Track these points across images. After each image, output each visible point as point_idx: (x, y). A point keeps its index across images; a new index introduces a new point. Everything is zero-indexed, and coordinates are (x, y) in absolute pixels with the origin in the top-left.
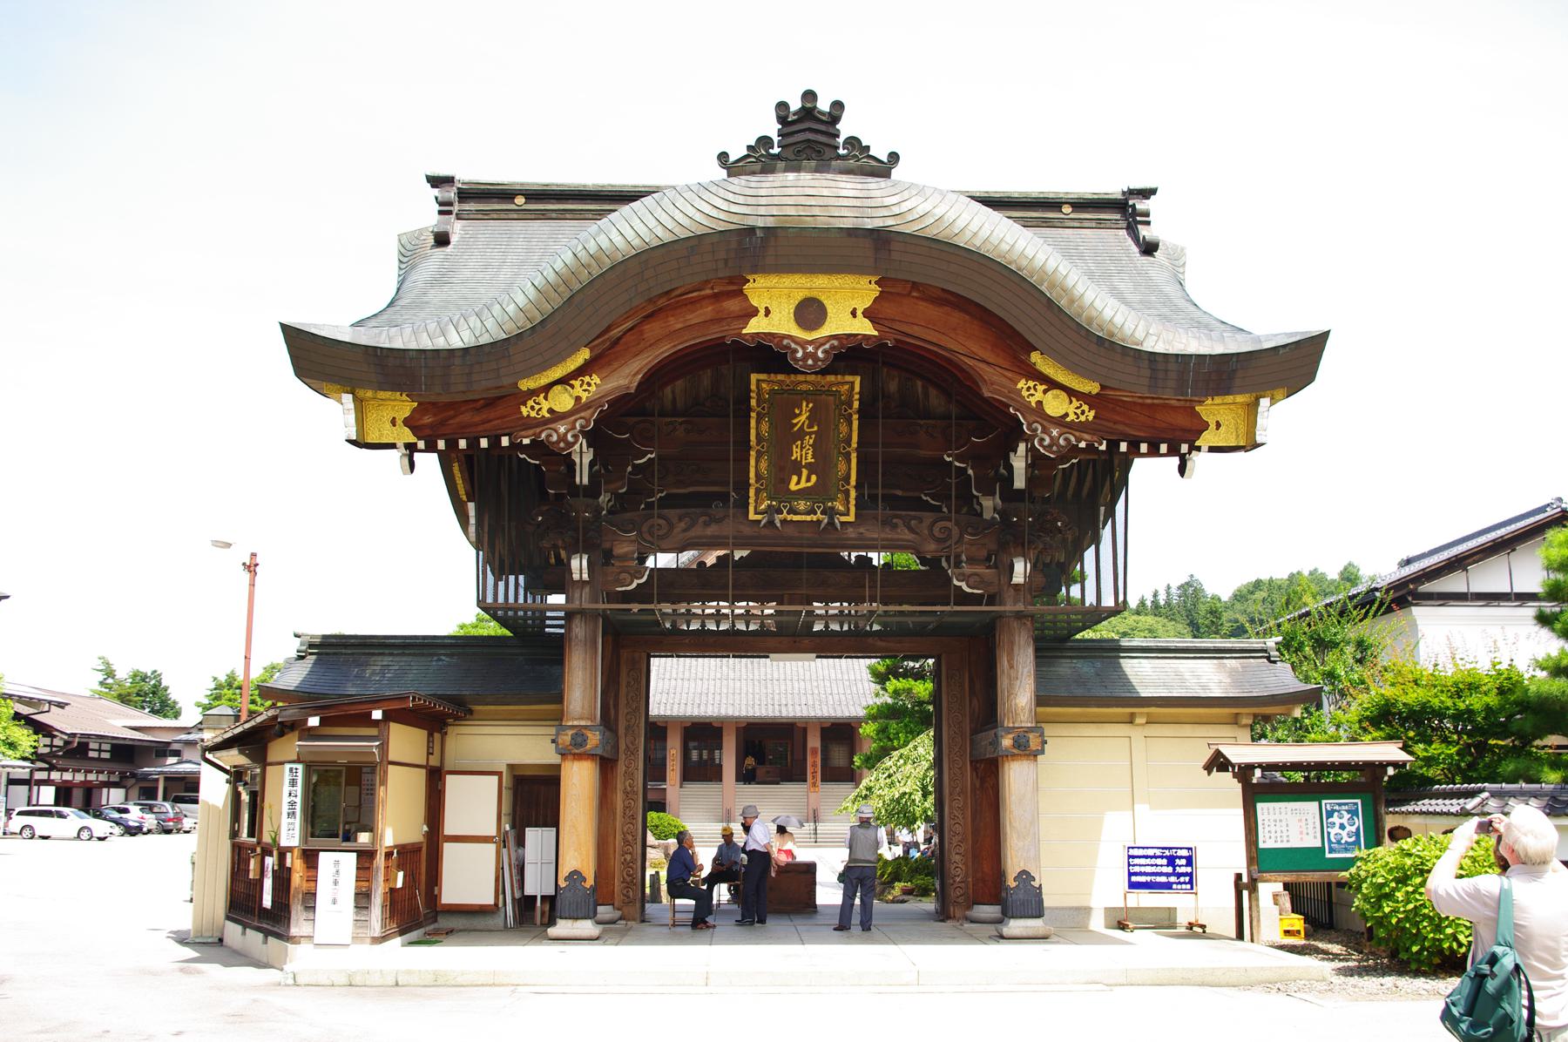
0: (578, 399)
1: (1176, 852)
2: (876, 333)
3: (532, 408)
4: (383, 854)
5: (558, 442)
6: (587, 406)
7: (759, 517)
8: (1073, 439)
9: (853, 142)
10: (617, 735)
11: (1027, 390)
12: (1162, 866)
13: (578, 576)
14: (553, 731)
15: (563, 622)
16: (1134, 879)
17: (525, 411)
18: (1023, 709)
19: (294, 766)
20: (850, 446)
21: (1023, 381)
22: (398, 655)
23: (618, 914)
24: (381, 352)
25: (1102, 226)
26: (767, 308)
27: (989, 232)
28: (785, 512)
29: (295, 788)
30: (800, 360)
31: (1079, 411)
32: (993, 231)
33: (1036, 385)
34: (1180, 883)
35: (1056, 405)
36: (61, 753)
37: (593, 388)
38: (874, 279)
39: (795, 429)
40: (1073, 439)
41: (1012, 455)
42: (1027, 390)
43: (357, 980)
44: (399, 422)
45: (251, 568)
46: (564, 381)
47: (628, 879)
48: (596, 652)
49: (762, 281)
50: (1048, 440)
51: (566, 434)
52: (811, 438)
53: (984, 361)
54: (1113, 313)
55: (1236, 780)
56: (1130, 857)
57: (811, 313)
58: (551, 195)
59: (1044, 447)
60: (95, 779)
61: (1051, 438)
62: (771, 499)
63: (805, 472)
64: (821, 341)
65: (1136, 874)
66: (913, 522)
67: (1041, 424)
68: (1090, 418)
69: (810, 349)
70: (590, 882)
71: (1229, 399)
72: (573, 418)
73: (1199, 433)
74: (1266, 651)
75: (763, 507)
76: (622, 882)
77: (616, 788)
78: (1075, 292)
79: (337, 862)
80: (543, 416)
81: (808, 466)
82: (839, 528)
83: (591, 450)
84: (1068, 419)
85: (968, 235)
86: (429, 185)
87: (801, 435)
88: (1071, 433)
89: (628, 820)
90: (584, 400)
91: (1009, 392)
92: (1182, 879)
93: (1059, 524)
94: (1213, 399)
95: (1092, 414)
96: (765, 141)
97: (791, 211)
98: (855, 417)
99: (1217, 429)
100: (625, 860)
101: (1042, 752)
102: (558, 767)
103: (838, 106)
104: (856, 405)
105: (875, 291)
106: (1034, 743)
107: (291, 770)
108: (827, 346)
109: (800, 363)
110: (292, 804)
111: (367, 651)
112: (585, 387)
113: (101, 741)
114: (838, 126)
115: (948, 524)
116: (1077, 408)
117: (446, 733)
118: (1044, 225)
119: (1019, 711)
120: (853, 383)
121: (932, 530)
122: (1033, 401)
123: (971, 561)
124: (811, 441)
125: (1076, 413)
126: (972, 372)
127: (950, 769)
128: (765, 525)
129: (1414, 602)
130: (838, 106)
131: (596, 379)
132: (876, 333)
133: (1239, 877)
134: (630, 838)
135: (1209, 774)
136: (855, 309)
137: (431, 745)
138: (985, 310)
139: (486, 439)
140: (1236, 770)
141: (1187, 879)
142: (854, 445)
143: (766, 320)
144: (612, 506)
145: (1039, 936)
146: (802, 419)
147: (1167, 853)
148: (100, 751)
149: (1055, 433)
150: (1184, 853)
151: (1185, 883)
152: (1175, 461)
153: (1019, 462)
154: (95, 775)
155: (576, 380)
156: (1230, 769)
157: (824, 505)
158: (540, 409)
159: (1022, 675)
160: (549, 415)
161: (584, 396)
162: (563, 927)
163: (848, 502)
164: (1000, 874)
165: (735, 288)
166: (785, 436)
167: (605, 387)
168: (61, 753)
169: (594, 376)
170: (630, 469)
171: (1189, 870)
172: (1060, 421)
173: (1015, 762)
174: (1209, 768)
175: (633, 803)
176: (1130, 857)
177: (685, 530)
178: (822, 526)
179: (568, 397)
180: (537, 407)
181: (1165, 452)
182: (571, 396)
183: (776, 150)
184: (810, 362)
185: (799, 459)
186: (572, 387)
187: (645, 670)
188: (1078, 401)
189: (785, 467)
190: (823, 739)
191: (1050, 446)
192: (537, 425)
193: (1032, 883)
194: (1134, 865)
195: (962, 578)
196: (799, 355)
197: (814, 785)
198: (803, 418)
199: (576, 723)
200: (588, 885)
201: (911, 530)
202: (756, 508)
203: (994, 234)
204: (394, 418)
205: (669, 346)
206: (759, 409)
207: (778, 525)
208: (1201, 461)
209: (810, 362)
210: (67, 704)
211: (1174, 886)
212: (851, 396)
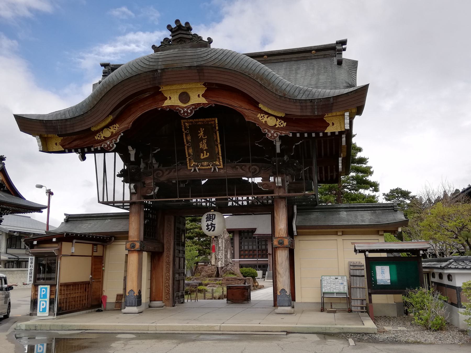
0: (112, 132)
3: (98, 137)
5: (107, 147)
7: (191, 168)
8: (279, 134)
15: (129, 207)
17: (96, 138)
19: (32, 257)
21: (259, 114)
23: (164, 304)
24: (45, 122)
25: (325, 57)
26: (170, 97)
29: (32, 265)
30: (183, 114)
31: (280, 123)
35: (271, 122)
37: (117, 129)
38: (202, 84)
39: (200, 138)
40: (279, 134)
42: (264, 119)
46: (108, 126)
47: (167, 292)
49: (165, 88)
52: (205, 140)
57: (184, 97)
61: (271, 134)
63: (205, 152)
64: (189, 106)
67: (267, 129)
68: (285, 126)
69: (185, 110)
71: (334, 114)
73: (326, 128)
74: (393, 207)
75: (218, 163)
77: (163, 261)
81: (205, 150)
84: (277, 127)
87: (202, 139)
90: (114, 133)
91: (255, 119)
93: (295, 164)
94: (328, 114)
95: (285, 123)
97: (170, 62)
98: (218, 132)
99: (333, 125)
104: (217, 128)
107: (31, 259)
112: (114, 128)
118: (305, 59)
121: (249, 170)
122: (263, 121)
124: (205, 141)
125: (279, 124)
126: (241, 113)
131: (117, 125)
132: (207, 102)
134: (168, 278)
136: (199, 94)
142: (219, 142)
143: (170, 101)
149: (272, 132)
155: (111, 126)
158: (101, 137)
160: (104, 139)
161: (114, 131)
166: (196, 141)
169: (285, 123)
170: (294, 147)
172: (274, 127)
177: (168, 174)
179: (109, 132)
180: (100, 136)
182: (110, 131)
184: (186, 114)
185: (202, 148)
186: (110, 128)
189: (198, 151)
191: (271, 137)
195: (261, 185)
196: (182, 112)
201: (243, 170)
202: (190, 165)
203: (240, 63)
204: (56, 143)
205: (140, 113)
209: (186, 114)
212: (215, 125)
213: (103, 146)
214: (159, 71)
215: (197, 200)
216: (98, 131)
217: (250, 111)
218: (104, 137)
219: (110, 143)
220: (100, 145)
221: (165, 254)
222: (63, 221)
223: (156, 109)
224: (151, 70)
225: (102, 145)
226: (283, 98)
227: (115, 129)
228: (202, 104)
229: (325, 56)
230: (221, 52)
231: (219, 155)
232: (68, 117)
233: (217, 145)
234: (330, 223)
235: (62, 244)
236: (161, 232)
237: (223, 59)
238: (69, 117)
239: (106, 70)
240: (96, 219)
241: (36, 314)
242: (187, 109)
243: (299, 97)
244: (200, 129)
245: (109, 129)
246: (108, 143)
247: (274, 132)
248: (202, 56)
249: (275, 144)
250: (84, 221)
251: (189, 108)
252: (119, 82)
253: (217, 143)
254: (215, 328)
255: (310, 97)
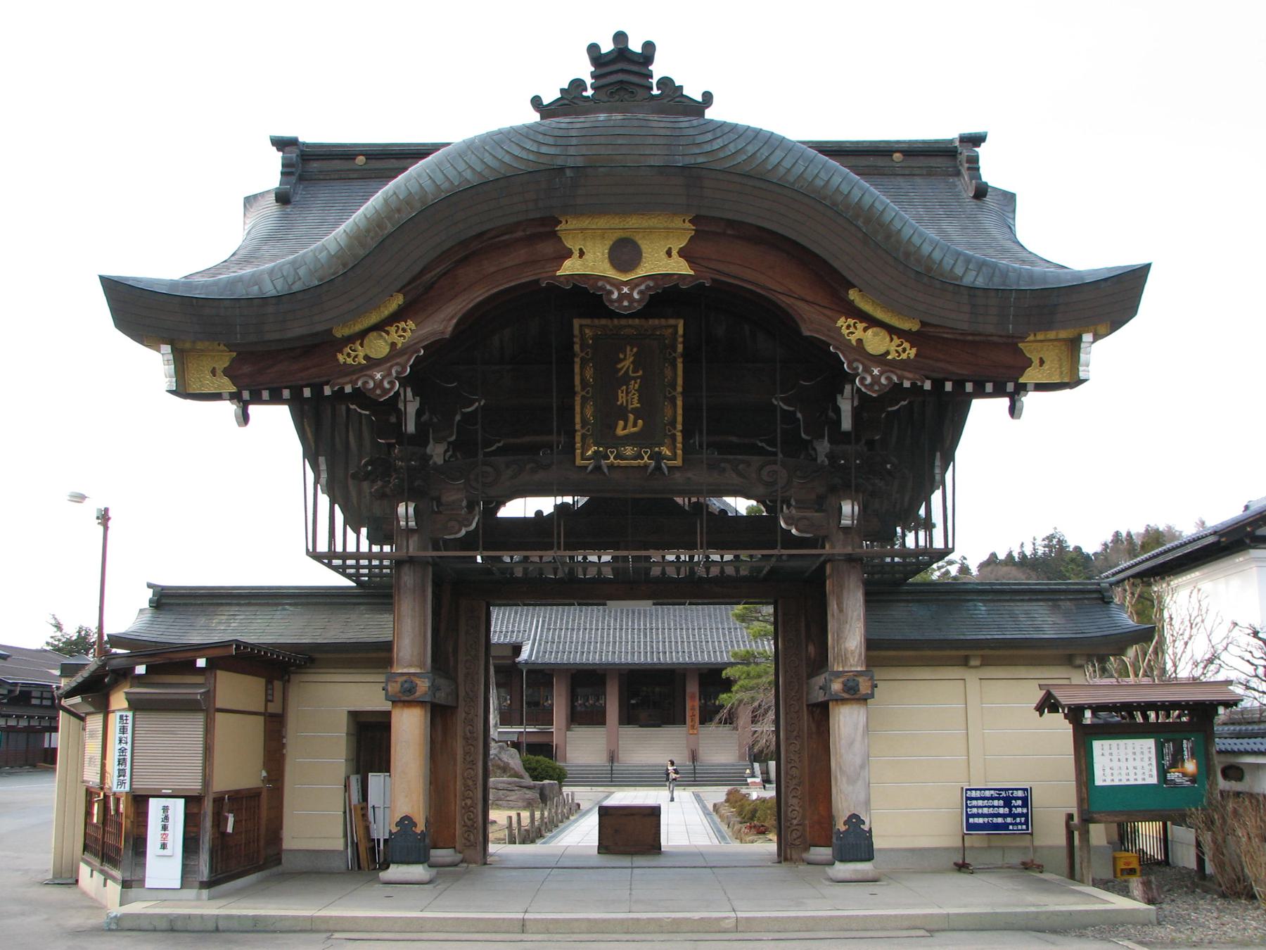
0: (393, 345)
1: (1012, 794)
2: (692, 273)
3: (349, 355)
4: (211, 800)
6: (403, 352)
8: (895, 378)
9: (666, 82)
10: (456, 683)
11: (846, 327)
12: (998, 807)
13: (404, 523)
14: (382, 678)
16: (971, 820)
18: (852, 652)
20: (675, 389)
22: (243, 605)
23: (459, 857)
27: (803, 168)
28: (612, 457)
29: (125, 735)
31: (900, 349)
32: (807, 167)
33: (856, 323)
34: (1016, 824)
35: (876, 342)
36: (5, 701)
40: (895, 378)
41: (839, 397)
43: (179, 925)
44: (219, 372)
45: (104, 518)
46: (380, 327)
47: (469, 823)
48: (425, 601)
50: (871, 379)
51: (382, 381)
52: (636, 383)
53: (802, 300)
54: (921, 241)
55: (1067, 721)
56: (968, 799)
57: (625, 253)
58: (392, 154)
59: (866, 386)
60: (37, 724)
61: (873, 376)
62: (598, 445)
63: (631, 417)
64: (636, 281)
65: (974, 816)
66: (741, 467)
67: (863, 364)
68: (912, 356)
69: (626, 290)
70: (421, 827)
71: (1052, 335)
72: (389, 364)
73: (1022, 370)
75: (590, 453)
76: (464, 826)
78: (893, 228)
79: (165, 809)
80: (359, 363)
81: (634, 411)
82: (666, 473)
83: (418, 398)
84: (889, 357)
85: (781, 171)
86: (275, 148)
87: (626, 380)
88: (892, 372)
89: (468, 766)
90: (399, 345)
92: (1018, 820)
93: (889, 466)
94: (1035, 335)
95: (914, 351)
96: (577, 84)
97: (603, 151)
98: (680, 360)
99: (1041, 365)
100: (466, 804)
101: (872, 696)
102: (388, 714)
103: (649, 47)
104: (680, 348)
105: (688, 230)
106: (864, 688)
107: (121, 717)
108: (643, 287)
109: (616, 304)
110: (123, 751)
111: (215, 601)
112: (401, 333)
113: (41, 689)
114: (650, 68)
115: (775, 467)
116: (898, 346)
117: (289, 681)
119: (849, 655)
120: (676, 327)
122: (853, 338)
123: (801, 505)
124: (637, 386)
125: (897, 351)
126: (790, 311)
127: (786, 714)
128: (591, 471)
129: (1252, 545)
130: (649, 47)
132: (692, 273)
133: (1070, 817)
134: (470, 783)
135: (1041, 715)
136: (670, 249)
137: (270, 692)
138: (803, 248)
139: (309, 389)
140: (1066, 711)
141: (1023, 819)
142: (680, 389)
143: (580, 262)
144: (451, 457)
145: (869, 879)
146: (626, 364)
147: (1003, 794)
148: (42, 698)
149: (876, 372)
150: (1020, 794)
151: (1021, 824)
152: (1005, 402)
153: (846, 406)
154: (16, 720)
155: (392, 326)
156: (1060, 711)
157: (590, 435)
158: (356, 356)
159: (852, 618)
161: (400, 343)
162: (396, 872)
163: (675, 447)
164: (830, 818)
165: (548, 229)
166: (609, 381)
167: (421, 332)
168: (5, 701)
170: (458, 418)
171: (1025, 811)
172: (881, 359)
173: (845, 706)
174: (1040, 709)
175: (472, 749)
176: (968, 799)
178: (649, 471)
180: (353, 354)
181: (991, 391)
182: (386, 341)
183: (589, 92)
185: (625, 404)
186: (388, 333)
187: (483, 618)
188: (899, 338)
189: (610, 414)
190: (701, 685)
191: (872, 385)
192: (353, 373)
193: (862, 826)
194: (971, 807)
196: (615, 296)
197: (693, 727)
198: (627, 363)
199: (405, 671)
200: (418, 831)
201: (739, 474)
202: (583, 454)
203: (809, 169)
204: (214, 368)
205: (484, 290)
206: (583, 354)
207: (606, 470)
208: (1031, 400)
210: (8, 656)
211: (1011, 827)
212: (675, 339)
213: (360, 384)
214: (569, 173)
215: (678, 558)
216: (350, 340)
217: (818, 308)
218: (367, 357)
219: (383, 378)
220: (350, 382)
221: (461, 715)
222: (146, 605)
223: (537, 282)
224: (543, 167)
225: (357, 379)
226: (925, 280)
227: (406, 333)
228: (676, 277)
229: (930, 173)
230: (752, 135)
231: (675, 428)
232: (270, 290)
233: (673, 401)
234: (954, 635)
235: (215, 675)
236: (451, 650)
237: (758, 154)
238: (274, 293)
239: (291, 159)
240: (247, 601)
241: (142, 882)
242: (632, 290)
243: (968, 280)
244: (626, 348)
245: (383, 334)
246: (378, 376)
247: (882, 373)
248: (700, 139)
249: (403, 409)
250: (211, 609)
251: (637, 285)
252: (443, 195)
253: (674, 393)
254: (721, 923)
255: (996, 283)
